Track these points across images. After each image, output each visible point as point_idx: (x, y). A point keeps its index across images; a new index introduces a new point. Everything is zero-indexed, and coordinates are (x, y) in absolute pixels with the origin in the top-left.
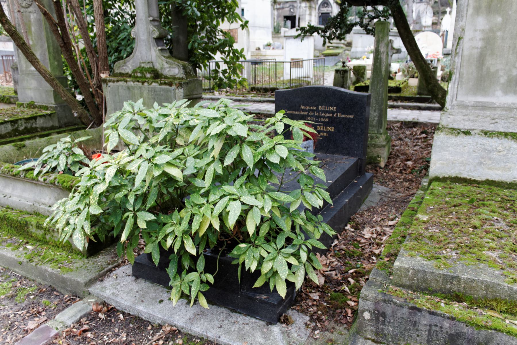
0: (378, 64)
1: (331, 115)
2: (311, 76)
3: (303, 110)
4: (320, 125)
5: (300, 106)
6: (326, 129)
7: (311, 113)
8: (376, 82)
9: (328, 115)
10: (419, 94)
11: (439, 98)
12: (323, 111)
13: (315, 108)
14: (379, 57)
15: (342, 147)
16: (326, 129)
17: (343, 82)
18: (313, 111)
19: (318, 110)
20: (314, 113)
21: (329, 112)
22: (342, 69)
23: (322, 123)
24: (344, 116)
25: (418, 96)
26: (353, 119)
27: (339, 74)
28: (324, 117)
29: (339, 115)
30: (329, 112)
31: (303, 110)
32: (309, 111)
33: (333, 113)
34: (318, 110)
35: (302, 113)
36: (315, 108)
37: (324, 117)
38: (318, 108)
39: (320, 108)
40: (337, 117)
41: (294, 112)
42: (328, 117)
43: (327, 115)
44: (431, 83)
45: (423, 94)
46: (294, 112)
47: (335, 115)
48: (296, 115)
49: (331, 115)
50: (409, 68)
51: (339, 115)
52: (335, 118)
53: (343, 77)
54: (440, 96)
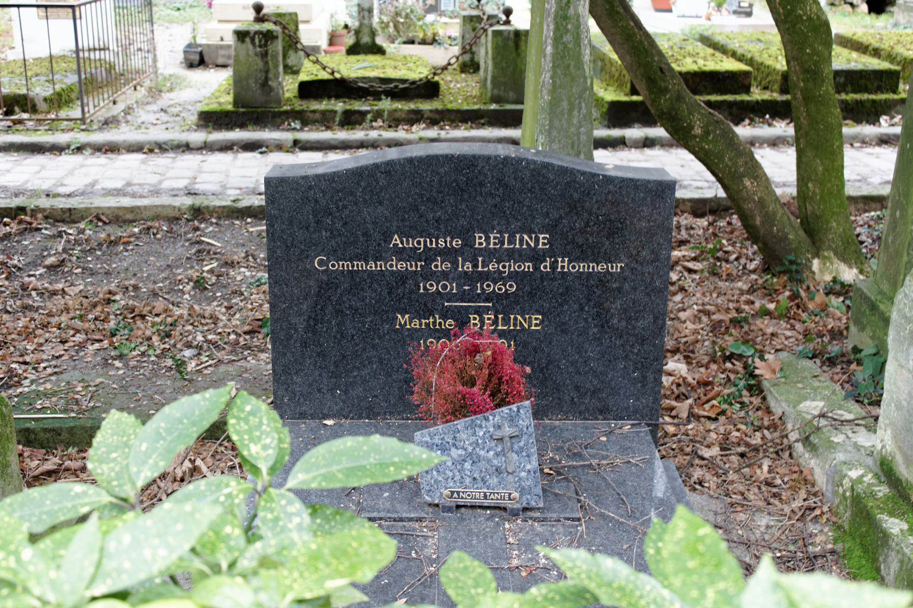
0: (568, 38)
1: (528, 266)
2: (113, 46)
3: (401, 254)
4: (479, 312)
5: (387, 238)
6: (506, 321)
7: (440, 265)
8: (565, 104)
9: (514, 267)
10: (495, 99)
11: (695, 136)
12: (490, 255)
13: (457, 243)
14: (571, 11)
15: (577, 388)
16: (506, 321)
17: (267, 72)
18: (448, 254)
19: (469, 251)
20: (455, 263)
21: (511, 255)
22: (257, 27)
23: (487, 300)
24: (582, 267)
25: (493, 107)
26: (622, 277)
27: (250, 47)
28: (497, 277)
29: (563, 264)
30: (511, 255)
31: (401, 254)
32: (429, 256)
33: (536, 257)
34: (469, 251)
35: (401, 266)
36: (457, 243)
37: (497, 277)
38: (468, 243)
39: (480, 241)
40: (553, 275)
41: (359, 265)
42: (514, 276)
43: (512, 267)
44: (666, 90)
45: (507, 102)
46: (359, 265)
47: (545, 266)
48: (371, 274)
49: (528, 266)
50: (398, 14)
51: (563, 264)
52: (544, 277)
53: (264, 55)
54: (698, 131)
